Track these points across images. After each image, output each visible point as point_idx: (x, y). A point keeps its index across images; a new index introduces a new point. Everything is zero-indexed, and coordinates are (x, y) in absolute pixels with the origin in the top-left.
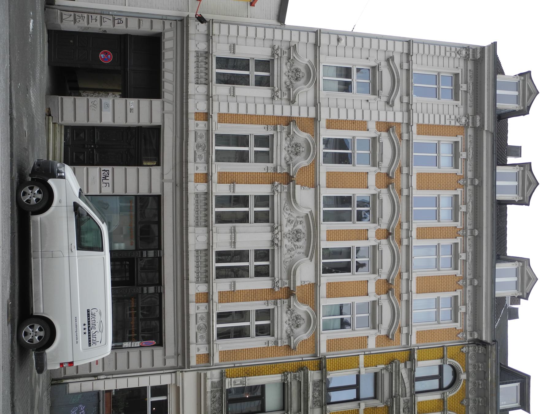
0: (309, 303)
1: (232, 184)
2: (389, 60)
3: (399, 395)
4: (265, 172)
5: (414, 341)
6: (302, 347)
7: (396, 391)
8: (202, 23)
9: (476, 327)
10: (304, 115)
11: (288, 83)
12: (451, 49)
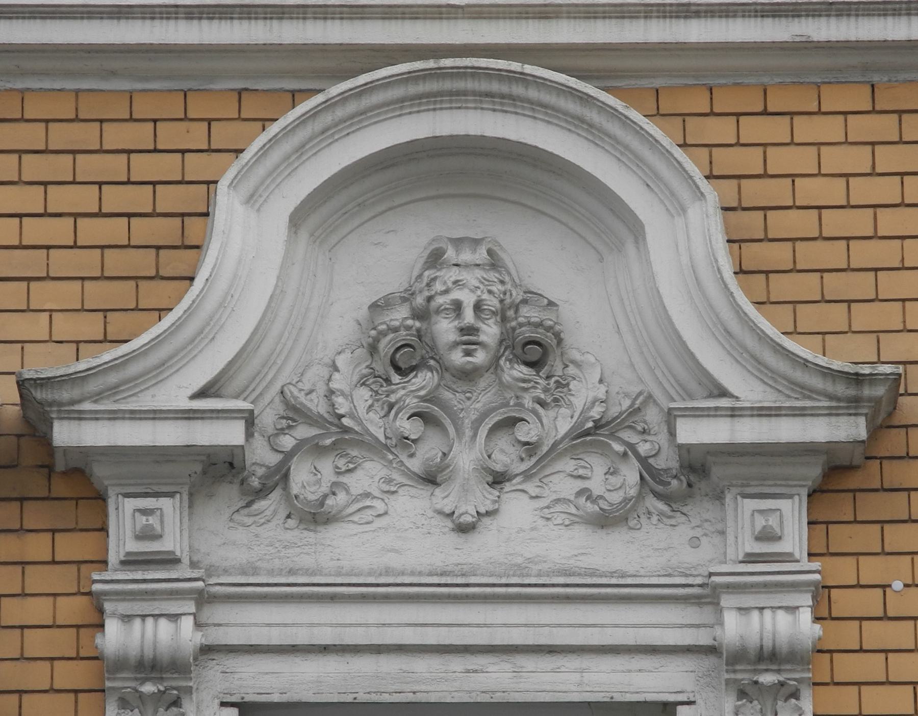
0: (197, 167)
6: (862, 285)
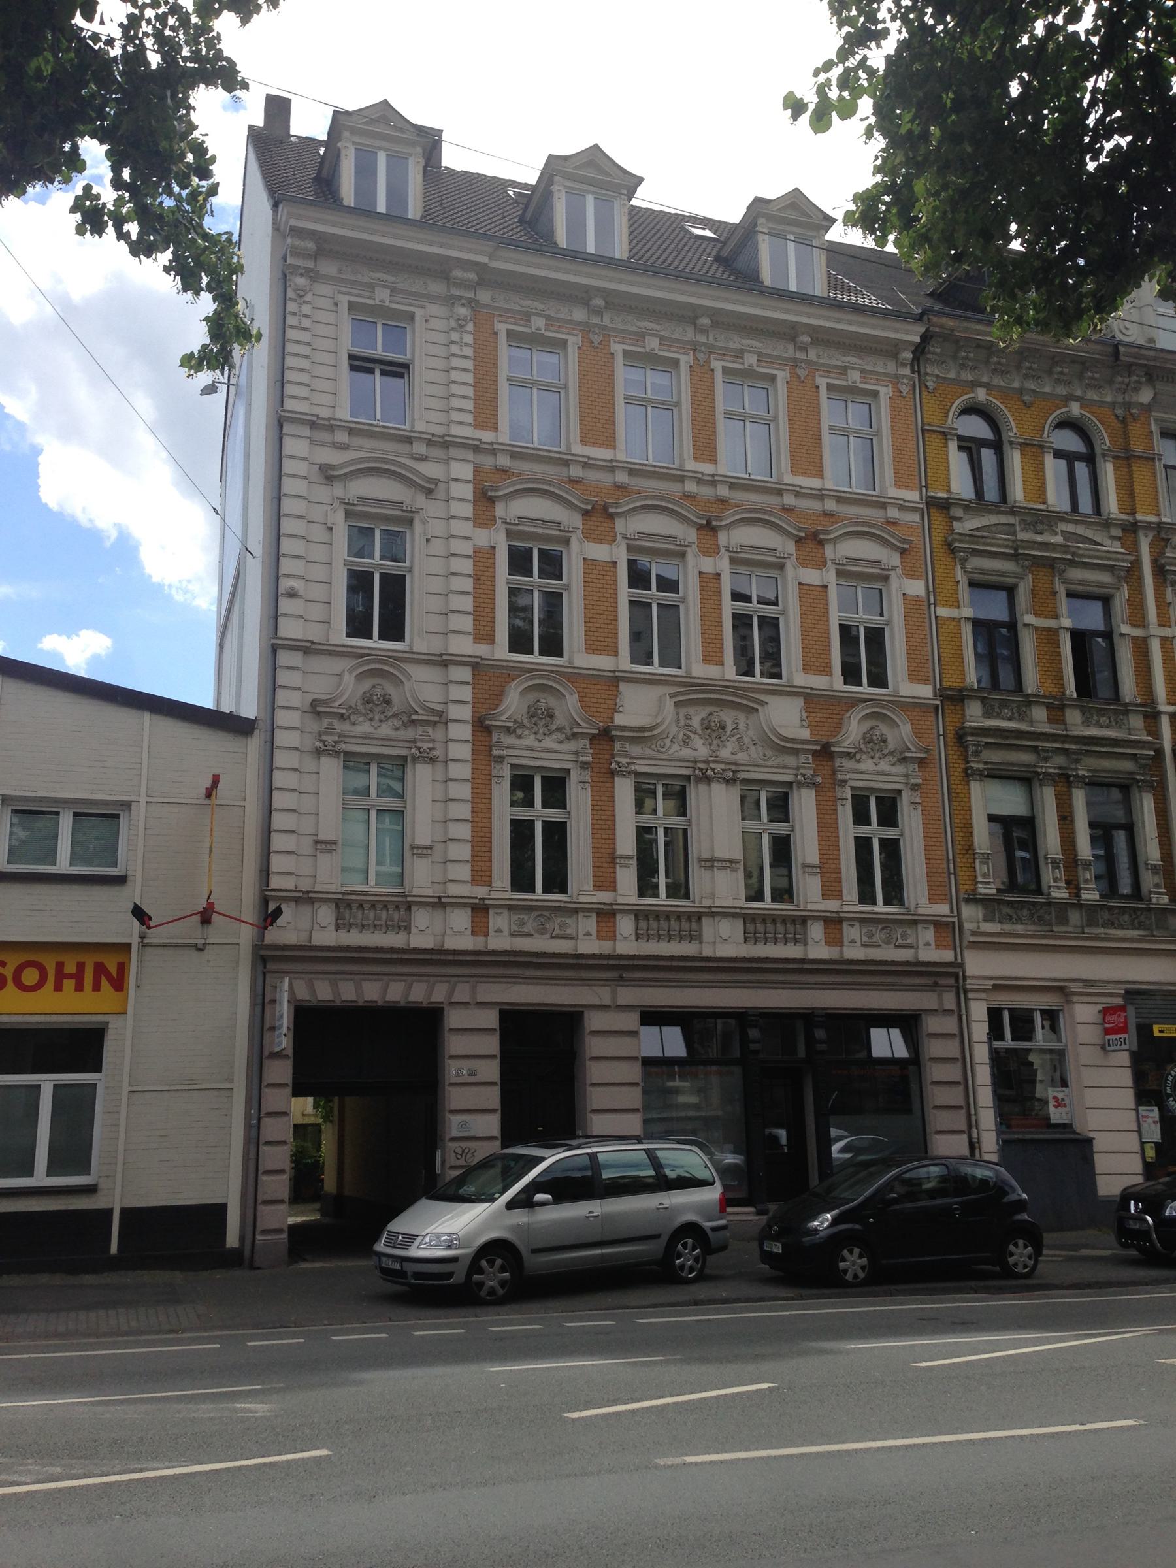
1: (618, 861)
2: (328, 475)
3: (1014, 541)
4: (589, 789)
5: (912, 496)
7: (1006, 547)
8: (281, 912)
9: (891, 350)
10: (466, 693)
11: (397, 723)
12: (294, 314)
